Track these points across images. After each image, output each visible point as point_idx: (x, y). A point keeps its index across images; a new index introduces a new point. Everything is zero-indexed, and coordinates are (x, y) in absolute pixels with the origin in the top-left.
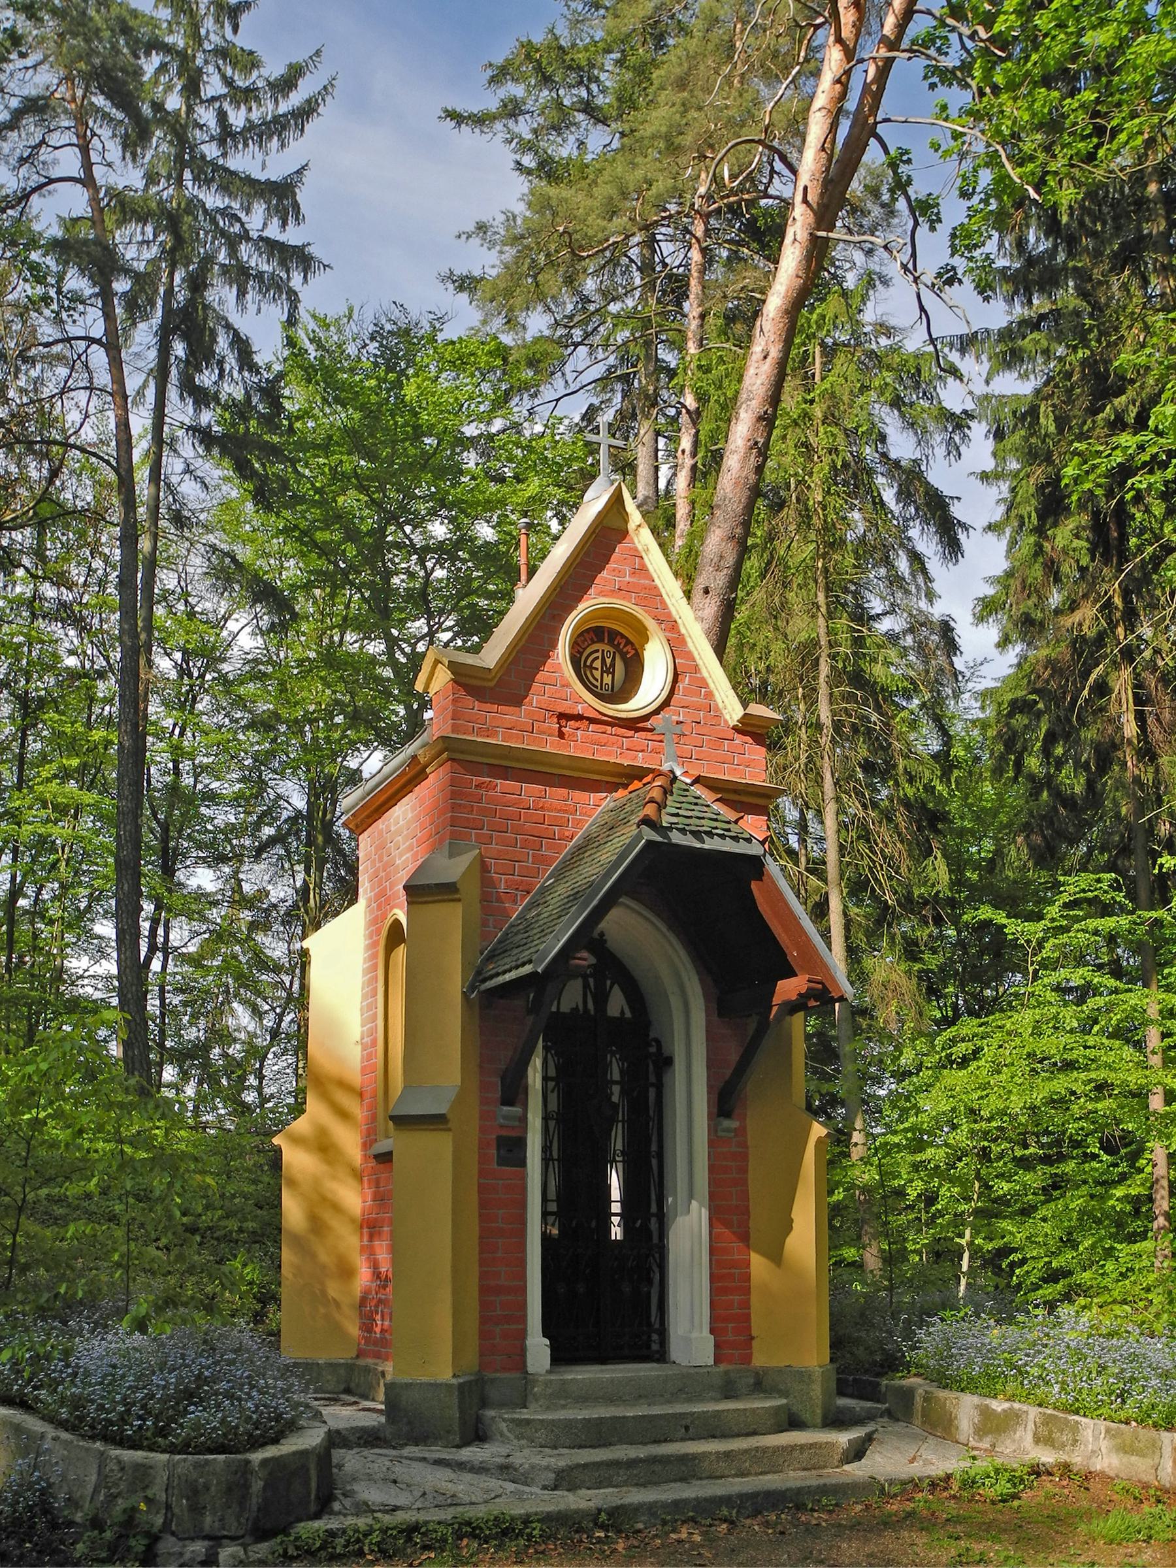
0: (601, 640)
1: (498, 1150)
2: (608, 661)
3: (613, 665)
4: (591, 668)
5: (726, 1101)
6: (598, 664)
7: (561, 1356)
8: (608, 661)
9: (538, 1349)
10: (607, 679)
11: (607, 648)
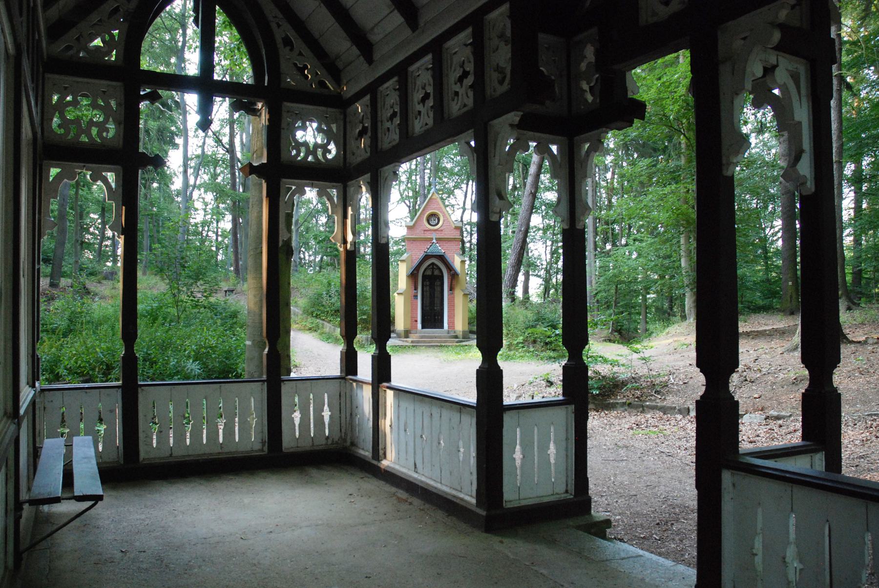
5: (451, 288)
7: (423, 328)
9: (419, 326)
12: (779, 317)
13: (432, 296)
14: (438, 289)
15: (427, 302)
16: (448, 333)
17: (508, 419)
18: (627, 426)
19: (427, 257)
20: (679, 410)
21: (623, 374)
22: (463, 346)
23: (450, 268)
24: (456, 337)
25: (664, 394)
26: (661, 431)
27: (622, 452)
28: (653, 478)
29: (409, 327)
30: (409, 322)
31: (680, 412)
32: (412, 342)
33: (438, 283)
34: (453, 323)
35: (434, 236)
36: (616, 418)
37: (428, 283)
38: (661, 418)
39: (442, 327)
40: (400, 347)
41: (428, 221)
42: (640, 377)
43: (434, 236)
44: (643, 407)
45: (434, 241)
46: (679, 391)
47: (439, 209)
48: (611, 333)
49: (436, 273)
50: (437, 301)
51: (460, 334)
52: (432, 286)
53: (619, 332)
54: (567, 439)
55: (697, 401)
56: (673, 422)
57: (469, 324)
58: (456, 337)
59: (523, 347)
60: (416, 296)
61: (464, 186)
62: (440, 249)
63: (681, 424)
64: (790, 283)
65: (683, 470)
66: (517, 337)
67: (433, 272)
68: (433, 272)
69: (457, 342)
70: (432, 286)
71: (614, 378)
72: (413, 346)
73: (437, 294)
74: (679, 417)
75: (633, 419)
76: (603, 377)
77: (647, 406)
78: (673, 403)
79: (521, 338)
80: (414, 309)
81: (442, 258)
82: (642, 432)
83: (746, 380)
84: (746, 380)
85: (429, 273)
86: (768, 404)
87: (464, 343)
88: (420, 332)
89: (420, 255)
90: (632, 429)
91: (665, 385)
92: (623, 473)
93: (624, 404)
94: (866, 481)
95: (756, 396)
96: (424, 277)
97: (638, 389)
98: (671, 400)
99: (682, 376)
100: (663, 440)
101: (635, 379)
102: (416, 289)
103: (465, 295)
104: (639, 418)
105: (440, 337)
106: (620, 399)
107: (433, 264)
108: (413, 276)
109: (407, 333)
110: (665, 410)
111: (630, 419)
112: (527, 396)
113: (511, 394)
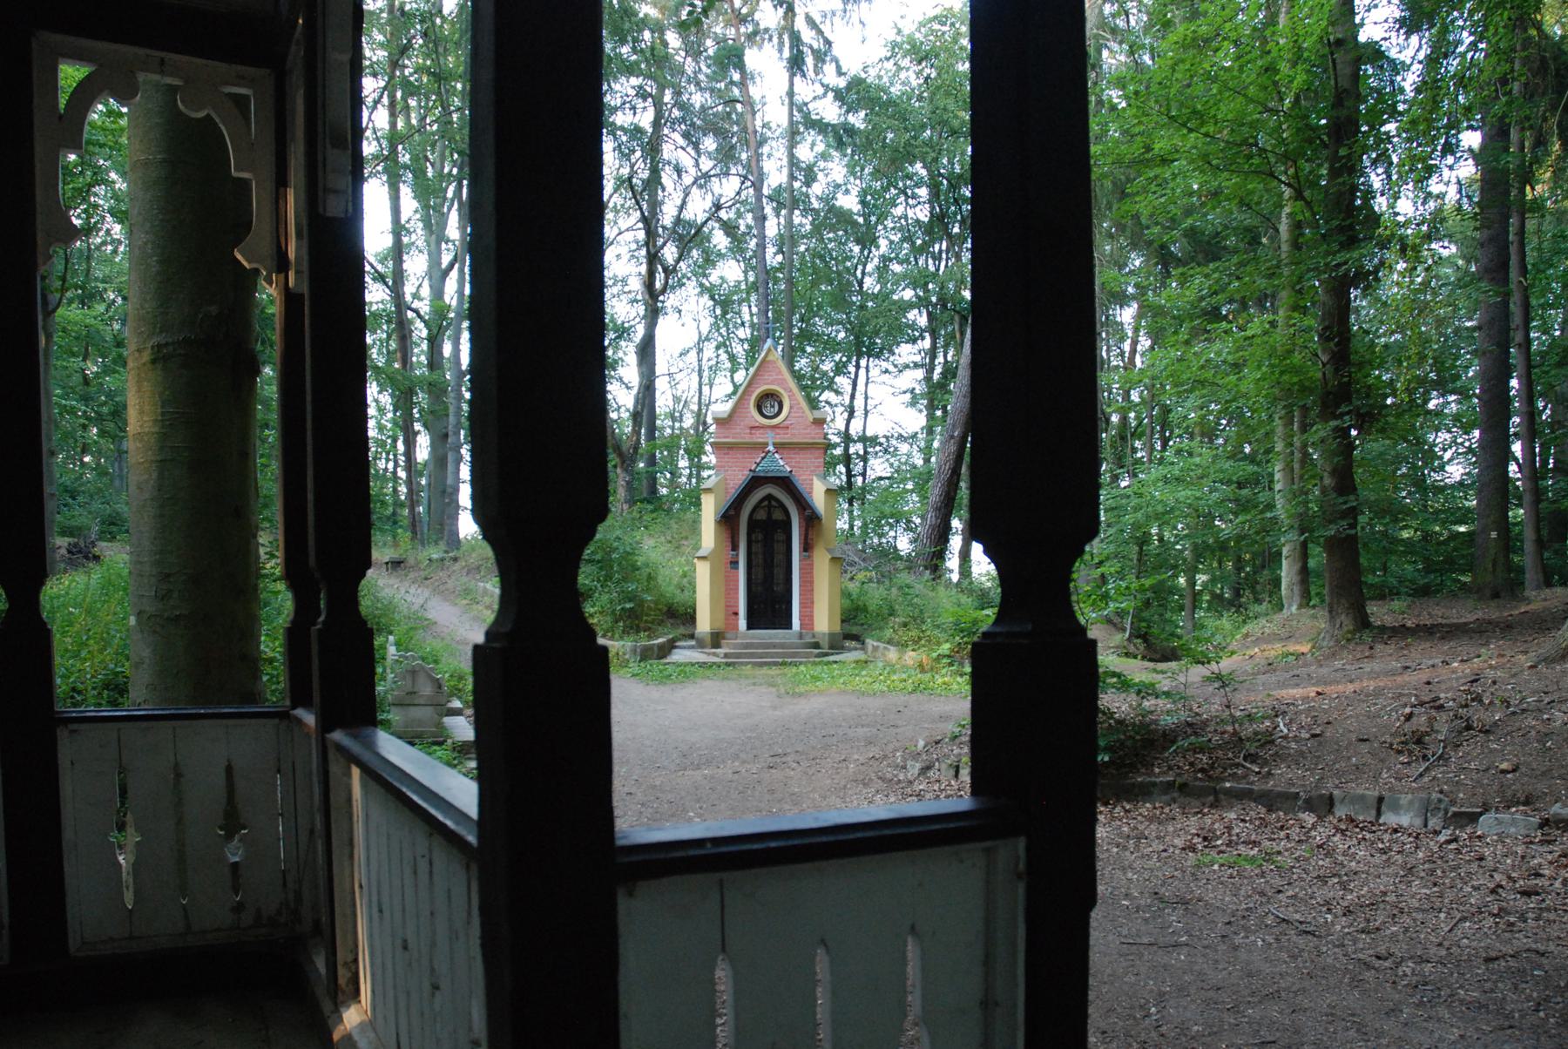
5: (807, 547)
7: (749, 628)
9: (742, 623)
12: (1470, 603)
13: (769, 565)
14: (779, 548)
15: (759, 574)
16: (801, 636)
17: (646, 927)
18: (1179, 842)
19: (755, 482)
20: (1307, 801)
21: (1166, 714)
22: (829, 663)
23: (803, 504)
24: (816, 645)
25: (1266, 763)
26: (1269, 856)
27: (1174, 917)
28: (1274, 1011)
29: (720, 625)
30: (721, 616)
31: (1309, 806)
32: (726, 655)
33: (780, 536)
34: (811, 617)
35: (770, 438)
36: (1151, 820)
37: (760, 537)
38: (1264, 823)
39: (789, 626)
40: (702, 665)
41: (759, 408)
42: (1205, 723)
43: (770, 438)
44: (1215, 792)
45: (771, 448)
46: (1302, 754)
47: (782, 382)
48: (1129, 640)
49: (778, 515)
50: (779, 573)
51: (825, 643)
52: (768, 543)
53: (1145, 637)
54: (987, 1004)
55: (476, 648)
56: (1295, 832)
57: (843, 621)
58: (816, 645)
59: (951, 664)
60: (735, 563)
61: (852, 369)
62: (781, 464)
63: (1318, 836)
64: (1494, 535)
65: (1356, 983)
66: (939, 644)
67: (769, 514)
68: (769, 514)
69: (818, 656)
70: (768, 543)
71: (1143, 725)
72: (728, 665)
73: (779, 558)
74: (1309, 818)
75: (1193, 824)
76: (1120, 722)
77: (1228, 792)
78: (1291, 783)
79: (947, 646)
80: (731, 590)
81: (785, 483)
82: (1222, 858)
83: (1469, 728)
84: (1469, 728)
85: (761, 515)
86: (1542, 787)
87: (831, 658)
88: (745, 637)
89: (739, 478)
90: (1193, 849)
91: (1267, 739)
92: (1182, 990)
93: (1170, 785)
94: (49, 395)
95: (1504, 766)
96: (753, 525)
97: (1202, 751)
98: (1284, 776)
99: (1305, 720)
100: (1277, 882)
101: (1194, 727)
102: (735, 547)
103: (834, 560)
104: (1208, 820)
105: (782, 646)
106: (1159, 774)
107: (769, 497)
108: (728, 519)
109: (716, 639)
110: (1272, 801)
111: (1187, 825)
112: (944, 766)
113: (909, 763)
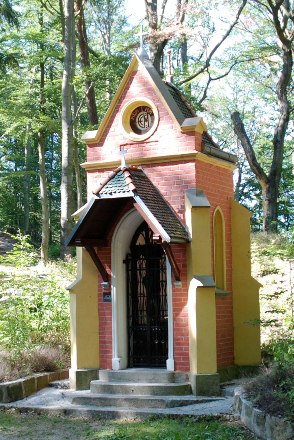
0: (140, 111)
1: (104, 297)
2: (146, 117)
3: (148, 118)
4: (141, 121)
6: (143, 119)
8: (146, 117)
9: (116, 361)
10: (146, 124)
11: (145, 112)
29: (94, 362)
